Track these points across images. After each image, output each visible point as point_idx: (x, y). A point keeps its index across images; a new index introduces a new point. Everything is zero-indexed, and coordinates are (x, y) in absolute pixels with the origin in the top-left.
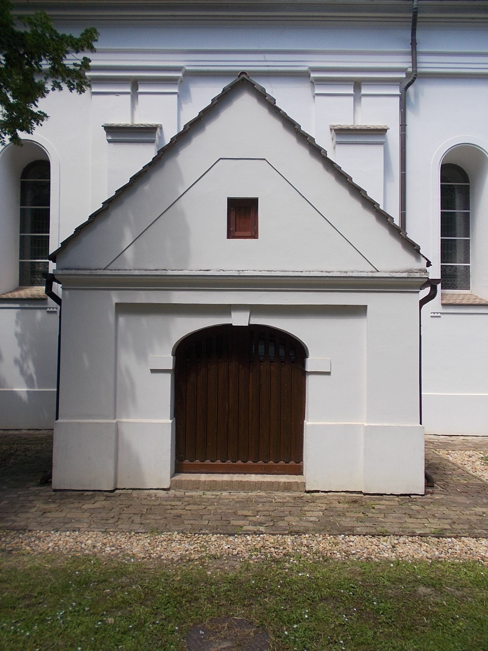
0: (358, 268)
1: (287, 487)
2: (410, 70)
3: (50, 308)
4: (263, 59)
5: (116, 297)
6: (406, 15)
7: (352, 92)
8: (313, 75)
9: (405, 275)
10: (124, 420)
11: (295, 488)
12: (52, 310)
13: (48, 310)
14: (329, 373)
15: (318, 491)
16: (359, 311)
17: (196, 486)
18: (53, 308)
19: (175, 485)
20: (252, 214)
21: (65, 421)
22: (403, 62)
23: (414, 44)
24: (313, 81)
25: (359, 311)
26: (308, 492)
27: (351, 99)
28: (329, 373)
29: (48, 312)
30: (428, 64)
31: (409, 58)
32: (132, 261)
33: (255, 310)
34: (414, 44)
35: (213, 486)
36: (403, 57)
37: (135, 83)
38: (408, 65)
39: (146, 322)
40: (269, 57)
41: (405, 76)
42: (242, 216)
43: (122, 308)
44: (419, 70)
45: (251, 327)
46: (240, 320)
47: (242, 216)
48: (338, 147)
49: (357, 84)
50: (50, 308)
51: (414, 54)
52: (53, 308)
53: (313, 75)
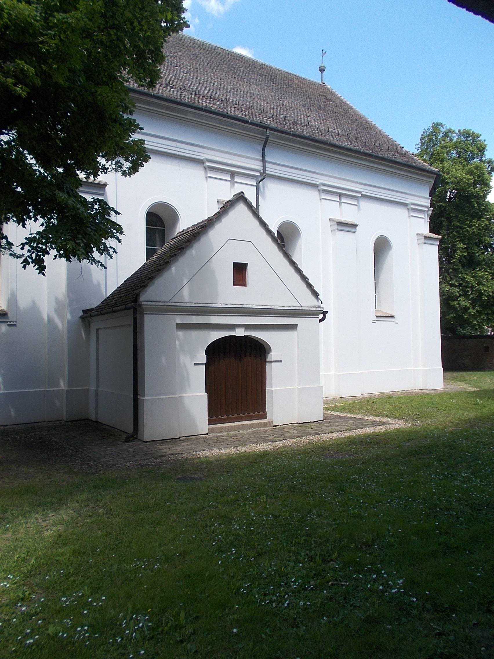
0: (294, 305)
1: (265, 425)
2: (262, 171)
3: (10, 322)
4: (175, 146)
5: (179, 319)
6: (263, 137)
7: (229, 179)
8: (208, 164)
9: (314, 309)
10: (184, 395)
11: (268, 425)
12: (12, 323)
13: (9, 323)
14: (281, 361)
15: (278, 425)
16: (293, 327)
17: (221, 430)
18: (13, 322)
19: (211, 431)
20: (244, 272)
21: (149, 398)
22: (258, 166)
23: (263, 156)
24: (207, 167)
25: (293, 327)
26: (274, 426)
27: (229, 183)
28: (281, 361)
29: (8, 325)
30: (271, 169)
31: (261, 164)
32: (186, 296)
33: (248, 327)
34: (263, 156)
35: (230, 429)
36: (256, 161)
37: (340, 195)
38: (261, 168)
39: (194, 334)
40: (179, 145)
41: (259, 175)
42: (240, 271)
43: (181, 326)
44: (267, 172)
45: (245, 337)
46: (240, 333)
47: (240, 271)
48: (338, 233)
49: (233, 174)
50: (10, 322)
51: (264, 161)
52: (13, 322)
53: (208, 164)
